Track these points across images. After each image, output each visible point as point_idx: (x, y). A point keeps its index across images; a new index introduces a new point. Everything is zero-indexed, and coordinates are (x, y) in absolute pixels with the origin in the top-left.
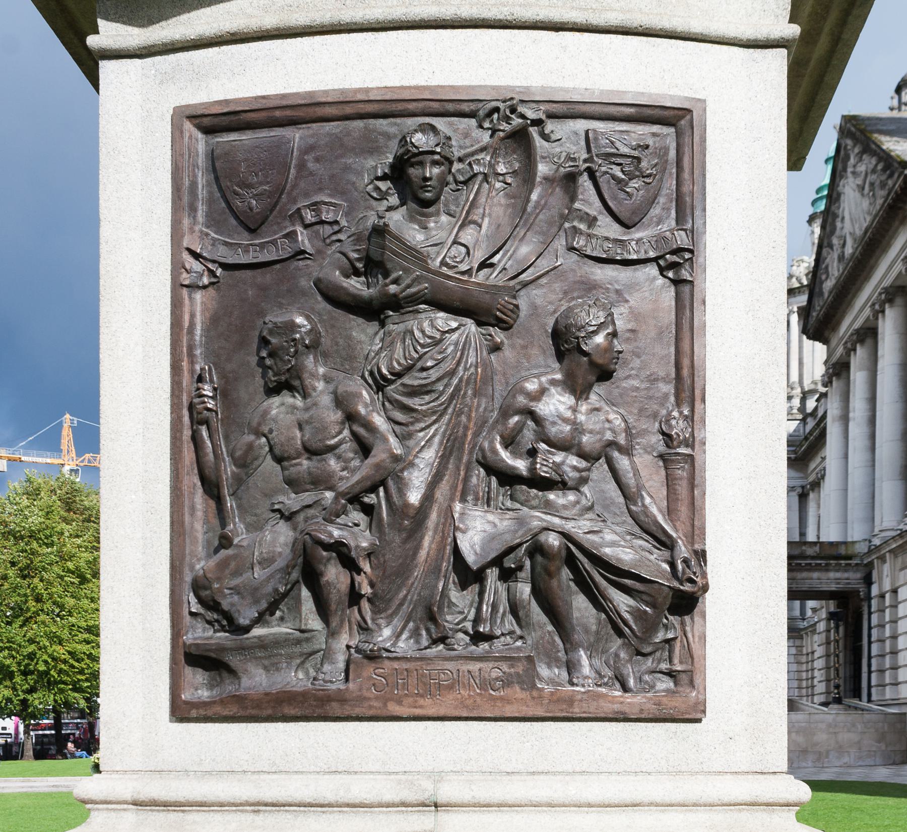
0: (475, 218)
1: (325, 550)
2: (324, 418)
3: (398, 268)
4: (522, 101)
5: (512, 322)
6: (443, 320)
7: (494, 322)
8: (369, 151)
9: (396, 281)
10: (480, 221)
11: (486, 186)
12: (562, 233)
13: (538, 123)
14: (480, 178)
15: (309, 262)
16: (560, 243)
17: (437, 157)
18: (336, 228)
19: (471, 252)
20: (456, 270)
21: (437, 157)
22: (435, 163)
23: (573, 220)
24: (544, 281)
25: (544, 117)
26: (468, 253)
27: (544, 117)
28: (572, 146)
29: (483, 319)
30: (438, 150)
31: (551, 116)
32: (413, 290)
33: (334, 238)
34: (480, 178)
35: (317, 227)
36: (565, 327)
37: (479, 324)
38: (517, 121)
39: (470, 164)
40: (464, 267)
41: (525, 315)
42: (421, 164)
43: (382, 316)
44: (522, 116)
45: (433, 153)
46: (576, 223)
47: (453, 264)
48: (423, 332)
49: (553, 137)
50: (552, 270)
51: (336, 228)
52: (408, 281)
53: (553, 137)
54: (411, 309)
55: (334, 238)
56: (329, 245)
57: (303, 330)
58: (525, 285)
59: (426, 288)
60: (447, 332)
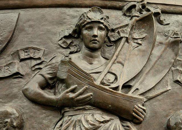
0: (121, 60)
1: (96, 39)
2: (148, 22)
3: (75, 83)
4: (148, 3)
5: (142, 119)
6: (99, 116)
7: (130, 119)
8: (61, 24)
9: (73, 91)
10: (123, 62)
11: (126, 43)
12: (170, 72)
13: (157, 14)
14: (124, 39)
15: (20, 79)
16: (170, 79)
17: (102, 25)
18: (39, 62)
19: (118, 78)
20: (110, 87)
21: (102, 25)
22: (100, 29)
23: (176, 66)
24: (159, 98)
25: (160, 12)
26: (116, 79)
27: (160, 12)
28: (175, 28)
29: (124, 116)
30: (102, 21)
31: (164, 12)
32: (81, 97)
33: (37, 67)
34: (124, 39)
35: (28, 61)
36: (175, 124)
37: (122, 119)
38: (145, 13)
39: (119, 33)
40: (113, 86)
41: (149, 116)
42: (91, 28)
43: (63, 112)
44: (148, 10)
45: (99, 22)
46: (178, 68)
47: (107, 83)
48: (87, 121)
49: (165, 23)
50: (165, 92)
51: (39, 62)
52: (81, 91)
53: (165, 23)
54: (81, 107)
55: (37, 67)
56: (34, 71)
57: (13, 116)
58: (149, 99)
59: (92, 95)
60: (102, 122)
